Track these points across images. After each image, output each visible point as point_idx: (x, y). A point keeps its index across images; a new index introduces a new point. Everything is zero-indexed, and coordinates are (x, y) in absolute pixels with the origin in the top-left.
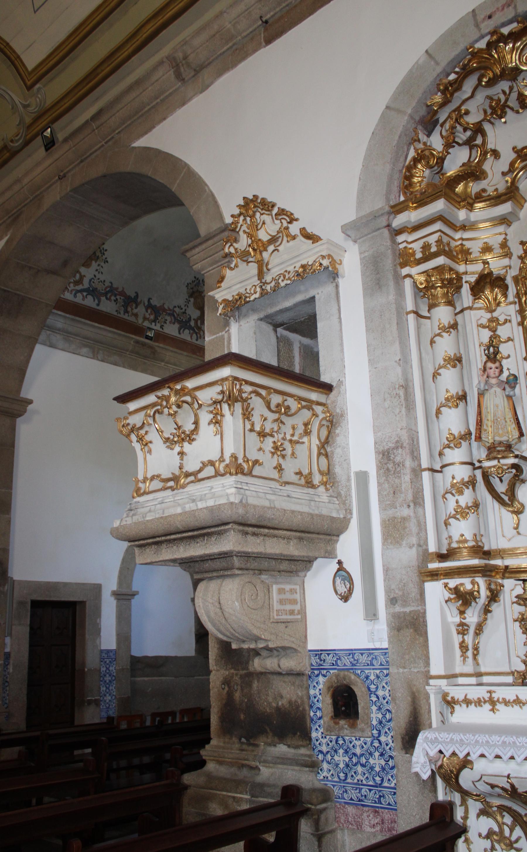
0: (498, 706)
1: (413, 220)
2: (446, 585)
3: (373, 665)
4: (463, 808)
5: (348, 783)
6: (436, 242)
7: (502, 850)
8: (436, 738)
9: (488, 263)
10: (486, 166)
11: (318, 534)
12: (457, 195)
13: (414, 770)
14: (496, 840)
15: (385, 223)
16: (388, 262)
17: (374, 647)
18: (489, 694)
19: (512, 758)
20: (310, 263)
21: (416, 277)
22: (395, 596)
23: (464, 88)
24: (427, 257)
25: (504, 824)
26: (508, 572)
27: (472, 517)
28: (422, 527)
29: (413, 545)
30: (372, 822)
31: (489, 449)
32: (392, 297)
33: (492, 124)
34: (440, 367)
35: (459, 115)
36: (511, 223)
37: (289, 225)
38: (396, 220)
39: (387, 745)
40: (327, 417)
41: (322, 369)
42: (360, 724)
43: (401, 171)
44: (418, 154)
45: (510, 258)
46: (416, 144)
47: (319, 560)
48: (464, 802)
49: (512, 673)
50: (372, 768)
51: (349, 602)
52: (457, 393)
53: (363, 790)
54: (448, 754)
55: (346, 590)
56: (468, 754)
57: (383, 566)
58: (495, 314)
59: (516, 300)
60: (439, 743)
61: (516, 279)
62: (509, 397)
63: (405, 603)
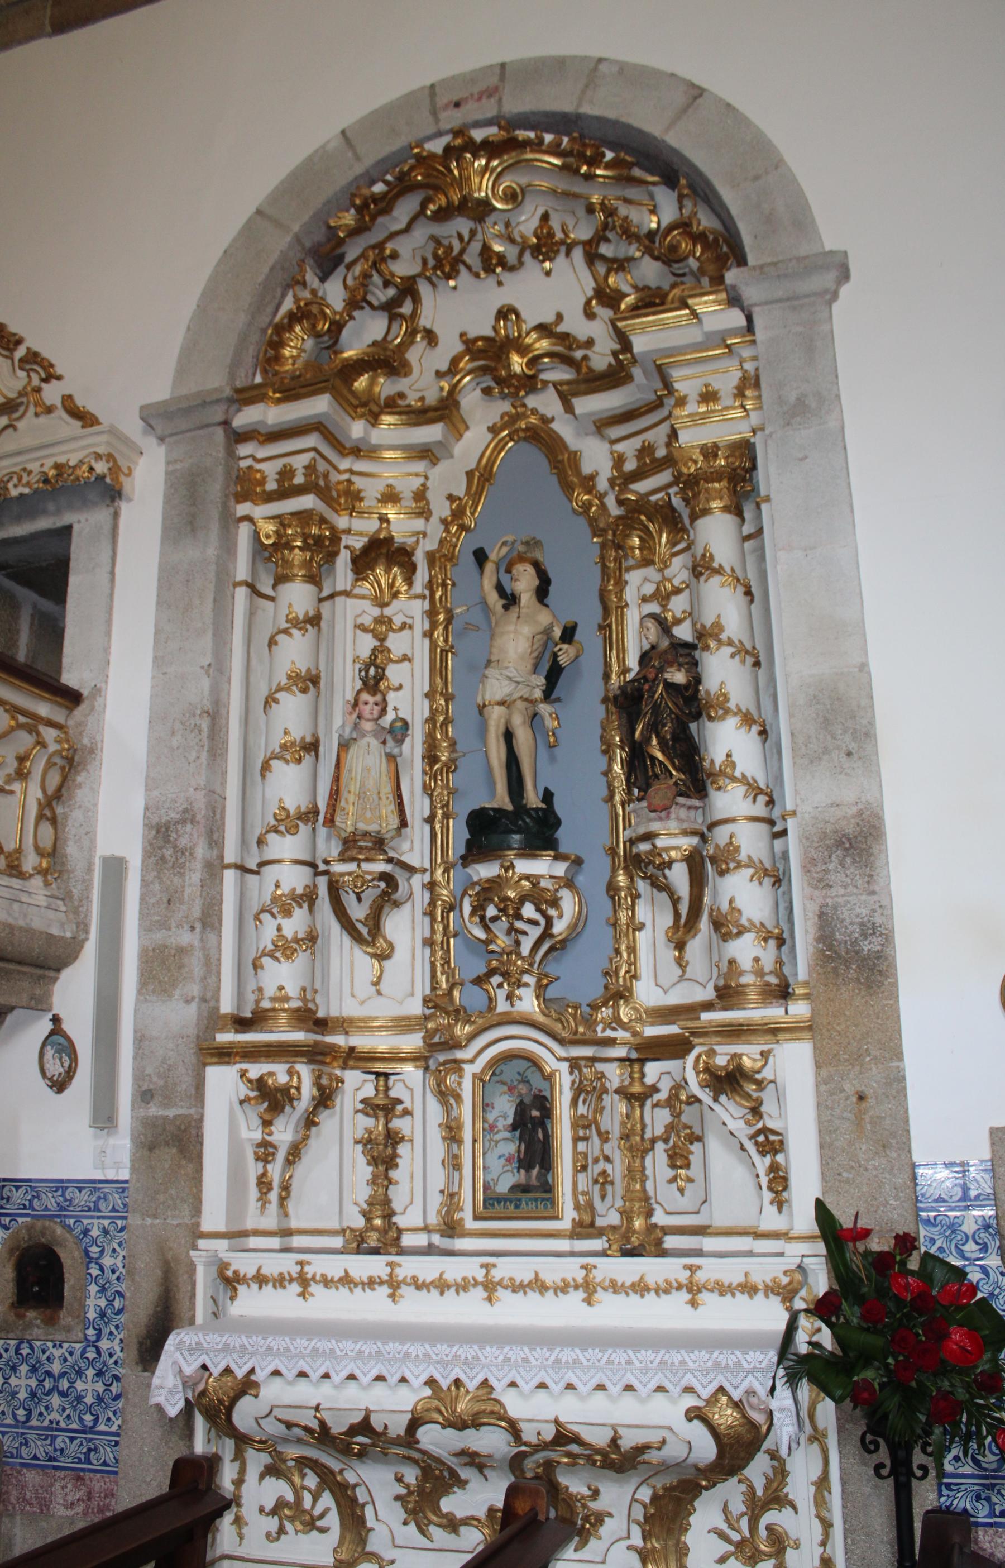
0: (313, 1288)
1: (270, 422)
2: (243, 1074)
3: (99, 1211)
4: (237, 1464)
5: (32, 1428)
6: (305, 467)
7: (297, 1532)
8: (198, 1343)
9: (388, 521)
10: (412, 355)
11: (20, 963)
12: (353, 393)
13: (154, 1401)
14: (288, 1517)
15: (220, 417)
16: (215, 488)
17: (103, 1178)
18: (299, 1267)
19: (326, 1376)
20: (72, 463)
21: (261, 523)
22: (152, 1087)
23: (396, 213)
24: (286, 491)
25: (303, 1488)
26: (352, 1057)
27: (302, 958)
28: (212, 967)
29: (193, 998)
30: (70, 1499)
31: (346, 842)
32: (212, 551)
33: (434, 285)
34: (279, 689)
35: (380, 257)
36: (438, 460)
37: (44, 385)
38: (240, 414)
39: (111, 1355)
40: (64, 749)
41: (66, 661)
42: (65, 1318)
43: (264, 331)
44: (299, 308)
45: (427, 520)
46: (298, 288)
47: (16, 1012)
48: (239, 1456)
49: (343, 1232)
50: (79, 1399)
51: (66, 1092)
52: (303, 739)
53: (59, 1440)
54: (216, 1371)
55: (62, 1070)
56: (252, 1371)
57: (135, 1032)
58: (388, 611)
59: (427, 593)
60: (206, 1351)
61: (431, 558)
62: (391, 758)
63: (168, 1101)
